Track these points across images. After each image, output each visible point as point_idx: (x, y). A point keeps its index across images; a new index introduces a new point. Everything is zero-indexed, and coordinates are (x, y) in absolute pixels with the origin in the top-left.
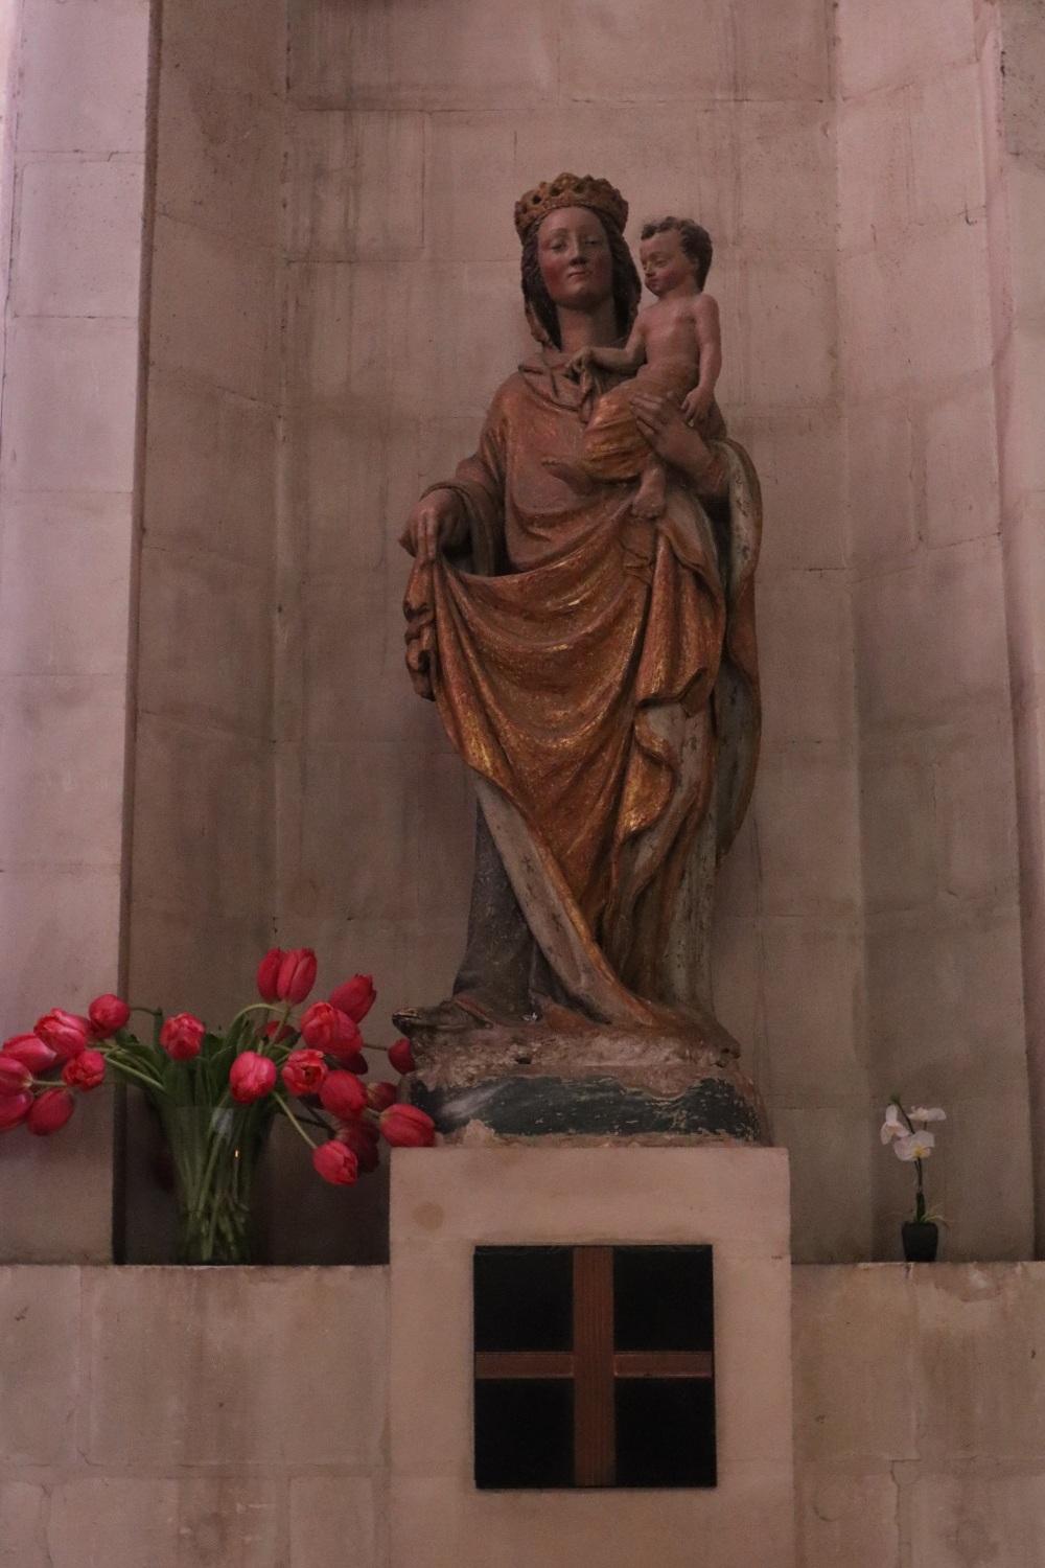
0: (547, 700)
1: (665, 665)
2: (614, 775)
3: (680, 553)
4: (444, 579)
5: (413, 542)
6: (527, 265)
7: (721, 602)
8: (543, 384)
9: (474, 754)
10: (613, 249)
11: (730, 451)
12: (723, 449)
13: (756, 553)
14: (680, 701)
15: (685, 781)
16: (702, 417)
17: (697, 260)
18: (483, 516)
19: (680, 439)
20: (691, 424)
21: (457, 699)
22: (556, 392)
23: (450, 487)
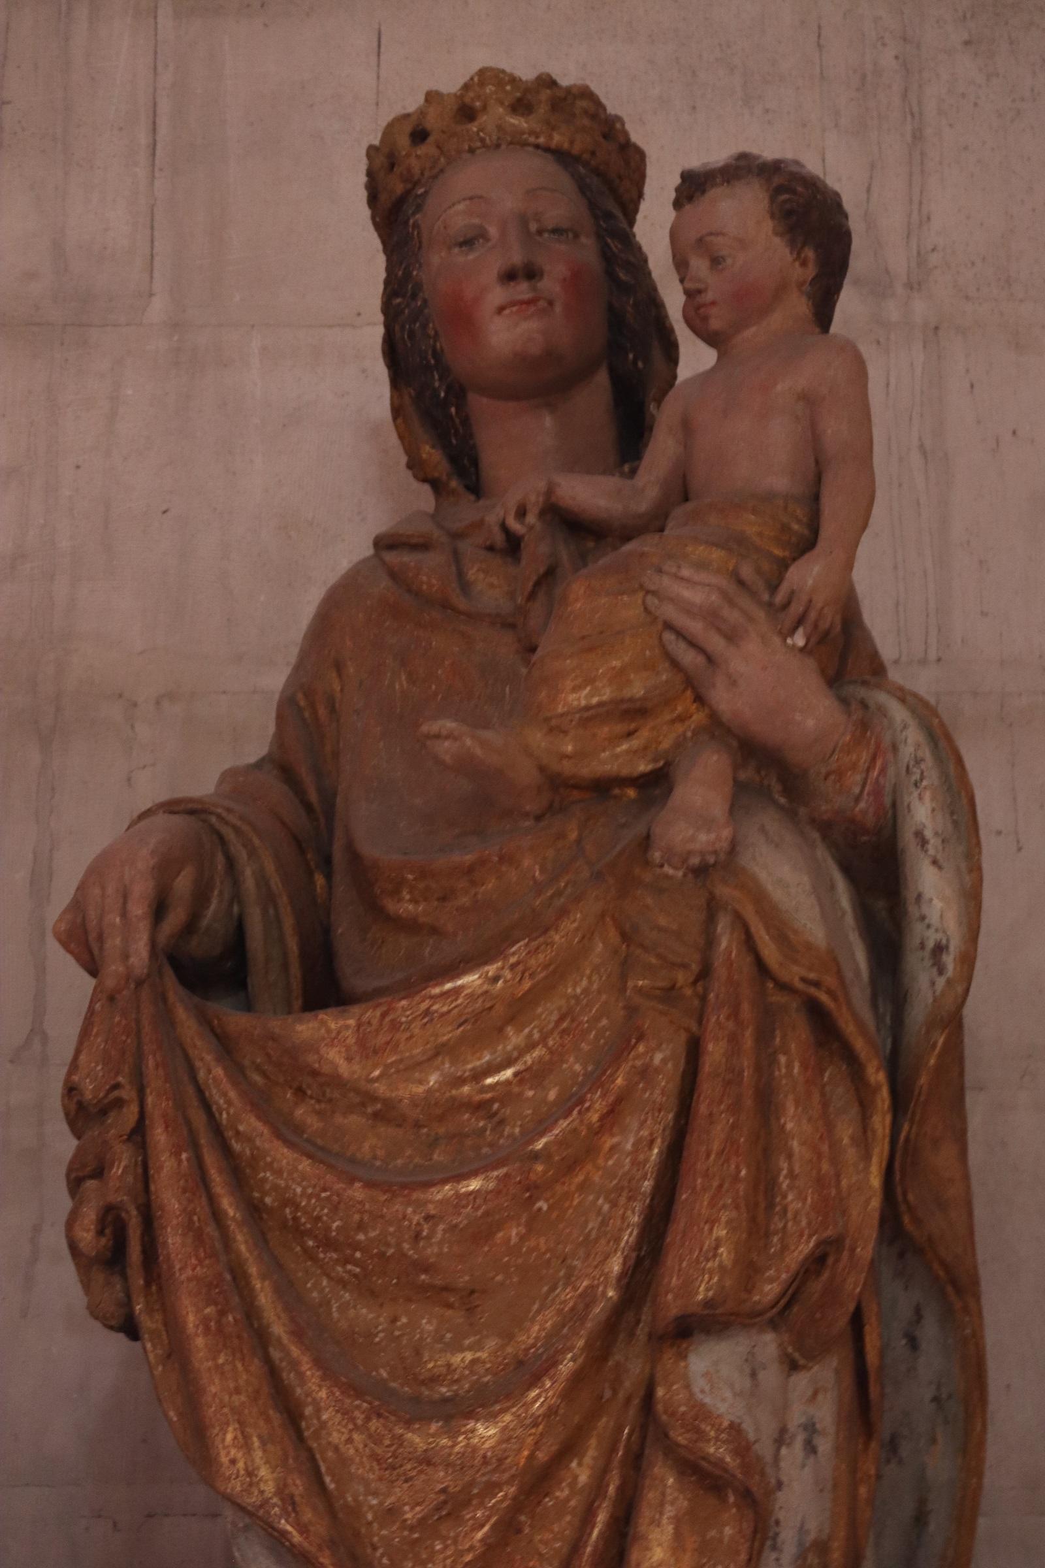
0: (428, 1326)
1: (731, 1225)
2: (601, 1518)
3: (770, 952)
4: (166, 1018)
5: (92, 936)
6: (395, 294)
7: (877, 1076)
8: (429, 569)
9: (233, 1462)
10: (607, 257)
11: (898, 713)
12: (882, 711)
13: (968, 960)
14: (773, 1325)
15: (788, 1537)
16: (824, 625)
17: (810, 253)
18: (276, 883)
19: (769, 680)
20: (799, 640)
21: (191, 1320)
22: (465, 587)
23: (191, 812)
